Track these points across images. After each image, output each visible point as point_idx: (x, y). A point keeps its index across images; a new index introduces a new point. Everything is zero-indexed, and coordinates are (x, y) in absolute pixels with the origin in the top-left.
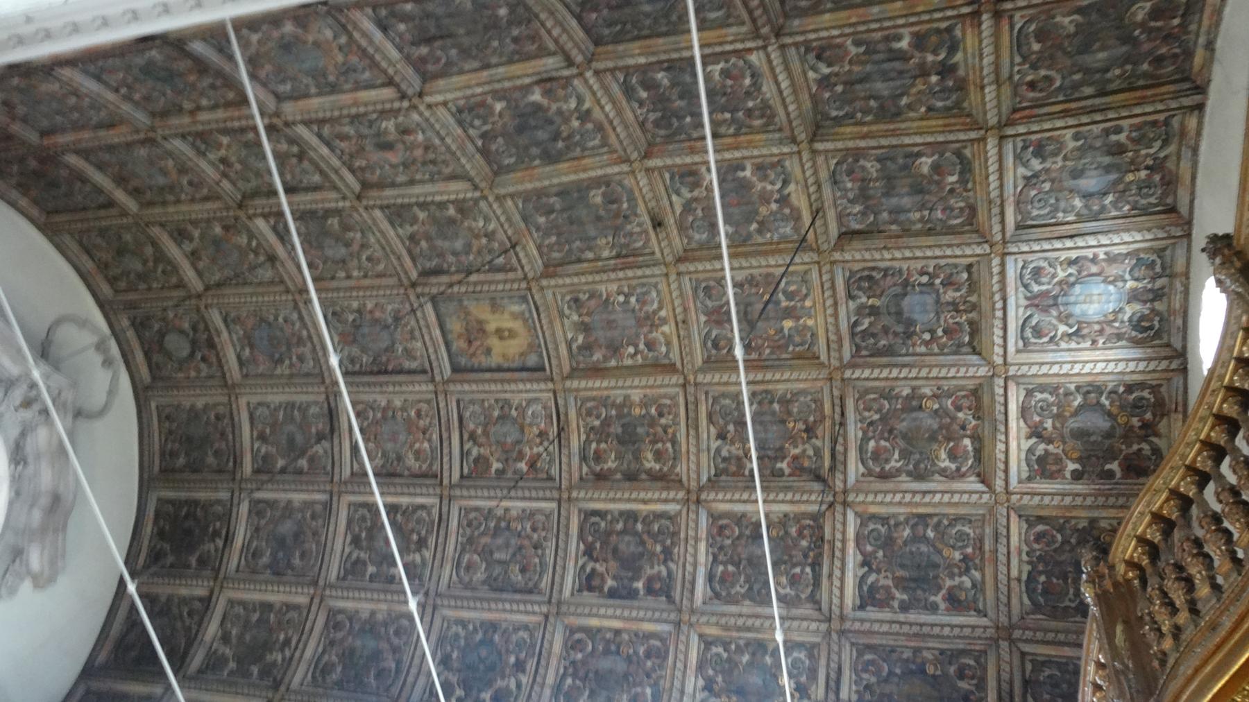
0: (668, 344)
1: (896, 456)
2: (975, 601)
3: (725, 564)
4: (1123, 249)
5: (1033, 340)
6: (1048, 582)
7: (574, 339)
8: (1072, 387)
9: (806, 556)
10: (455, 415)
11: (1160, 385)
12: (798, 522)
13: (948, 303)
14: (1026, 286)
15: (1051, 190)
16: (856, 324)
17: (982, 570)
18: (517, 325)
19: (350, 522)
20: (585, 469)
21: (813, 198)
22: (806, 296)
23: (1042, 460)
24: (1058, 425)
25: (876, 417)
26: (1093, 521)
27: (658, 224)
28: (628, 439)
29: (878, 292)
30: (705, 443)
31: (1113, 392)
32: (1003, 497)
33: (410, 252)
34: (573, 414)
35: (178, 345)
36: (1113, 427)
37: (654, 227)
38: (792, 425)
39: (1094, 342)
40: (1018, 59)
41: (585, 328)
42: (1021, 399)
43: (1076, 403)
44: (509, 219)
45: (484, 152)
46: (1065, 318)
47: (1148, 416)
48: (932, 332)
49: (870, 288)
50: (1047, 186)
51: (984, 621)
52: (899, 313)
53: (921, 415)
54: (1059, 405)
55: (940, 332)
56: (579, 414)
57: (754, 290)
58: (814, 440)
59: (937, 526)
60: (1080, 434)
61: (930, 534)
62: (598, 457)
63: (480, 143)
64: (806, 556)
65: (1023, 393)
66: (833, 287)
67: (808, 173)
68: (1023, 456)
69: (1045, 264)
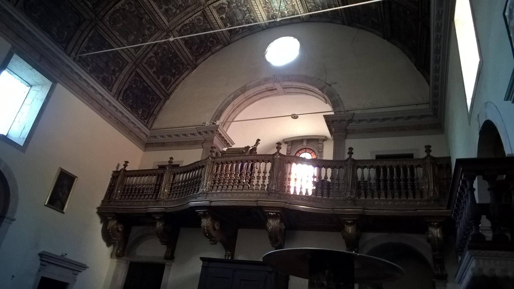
2: (170, 16)
4: (296, 8)
6: (188, 29)
17: (181, 12)
31: (251, 16)
32: (206, 5)
39: (265, 7)
51: (167, 24)
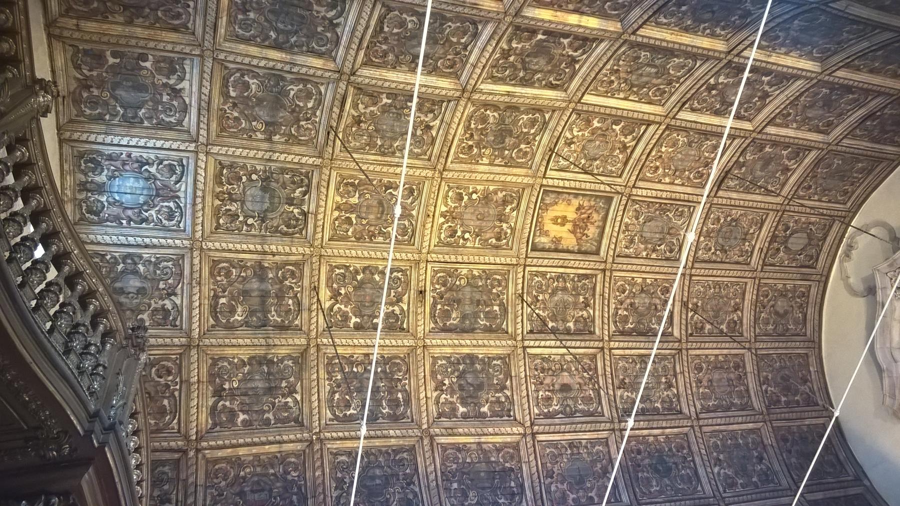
0: (446, 196)
1: (292, 93)
3: (459, 43)
5: (175, 163)
7: (513, 210)
8: (146, 124)
9: (386, 39)
10: (628, 168)
11: (76, 116)
12: (384, 62)
13: (236, 201)
14: (179, 207)
15: (159, 281)
16: (305, 194)
18: (549, 226)
19: (759, 110)
20: (547, 116)
21: (315, 300)
22: (336, 219)
23: (173, 71)
24: (158, 96)
25: (303, 123)
26: (129, 22)
27: (422, 293)
28: (503, 132)
29: (285, 214)
30: (443, 127)
33: (594, 295)
34: (538, 158)
35: (797, 242)
36: (114, 90)
37: (425, 291)
38: (370, 128)
40: (177, 394)
41: (502, 218)
42: (187, 119)
43: (143, 111)
44: (516, 317)
45: (508, 375)
46: (150, 178)
47: (85, 95)
48: (250, 180)
49: (290, 219)
50: (162, 286)
52: (272, 197)
53: (267, 119)
54: (155, 110)
55: (244, 179)
56: (534, 155)
57: (372, 229)
58: (356, 114)
59: (268, 37)
60: (140, 88)
61: (273, 34)
62: (533, 123)
63: (508, 383)
64: (386, 39)
65: (185, 123)
66: (315, 226)
67: (315, 320)
68: (188, 76)
69: (164, 222)
